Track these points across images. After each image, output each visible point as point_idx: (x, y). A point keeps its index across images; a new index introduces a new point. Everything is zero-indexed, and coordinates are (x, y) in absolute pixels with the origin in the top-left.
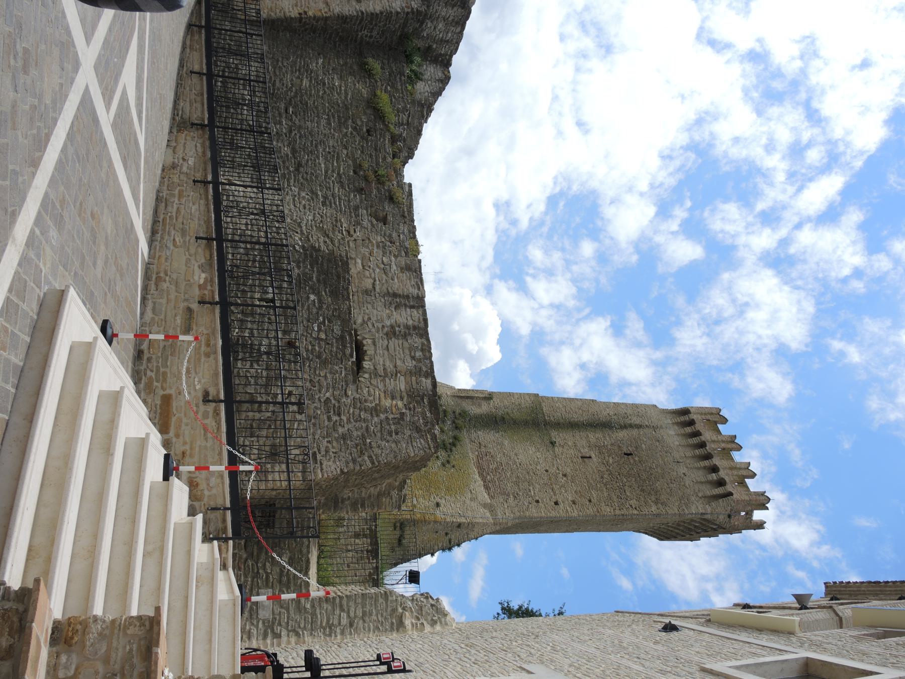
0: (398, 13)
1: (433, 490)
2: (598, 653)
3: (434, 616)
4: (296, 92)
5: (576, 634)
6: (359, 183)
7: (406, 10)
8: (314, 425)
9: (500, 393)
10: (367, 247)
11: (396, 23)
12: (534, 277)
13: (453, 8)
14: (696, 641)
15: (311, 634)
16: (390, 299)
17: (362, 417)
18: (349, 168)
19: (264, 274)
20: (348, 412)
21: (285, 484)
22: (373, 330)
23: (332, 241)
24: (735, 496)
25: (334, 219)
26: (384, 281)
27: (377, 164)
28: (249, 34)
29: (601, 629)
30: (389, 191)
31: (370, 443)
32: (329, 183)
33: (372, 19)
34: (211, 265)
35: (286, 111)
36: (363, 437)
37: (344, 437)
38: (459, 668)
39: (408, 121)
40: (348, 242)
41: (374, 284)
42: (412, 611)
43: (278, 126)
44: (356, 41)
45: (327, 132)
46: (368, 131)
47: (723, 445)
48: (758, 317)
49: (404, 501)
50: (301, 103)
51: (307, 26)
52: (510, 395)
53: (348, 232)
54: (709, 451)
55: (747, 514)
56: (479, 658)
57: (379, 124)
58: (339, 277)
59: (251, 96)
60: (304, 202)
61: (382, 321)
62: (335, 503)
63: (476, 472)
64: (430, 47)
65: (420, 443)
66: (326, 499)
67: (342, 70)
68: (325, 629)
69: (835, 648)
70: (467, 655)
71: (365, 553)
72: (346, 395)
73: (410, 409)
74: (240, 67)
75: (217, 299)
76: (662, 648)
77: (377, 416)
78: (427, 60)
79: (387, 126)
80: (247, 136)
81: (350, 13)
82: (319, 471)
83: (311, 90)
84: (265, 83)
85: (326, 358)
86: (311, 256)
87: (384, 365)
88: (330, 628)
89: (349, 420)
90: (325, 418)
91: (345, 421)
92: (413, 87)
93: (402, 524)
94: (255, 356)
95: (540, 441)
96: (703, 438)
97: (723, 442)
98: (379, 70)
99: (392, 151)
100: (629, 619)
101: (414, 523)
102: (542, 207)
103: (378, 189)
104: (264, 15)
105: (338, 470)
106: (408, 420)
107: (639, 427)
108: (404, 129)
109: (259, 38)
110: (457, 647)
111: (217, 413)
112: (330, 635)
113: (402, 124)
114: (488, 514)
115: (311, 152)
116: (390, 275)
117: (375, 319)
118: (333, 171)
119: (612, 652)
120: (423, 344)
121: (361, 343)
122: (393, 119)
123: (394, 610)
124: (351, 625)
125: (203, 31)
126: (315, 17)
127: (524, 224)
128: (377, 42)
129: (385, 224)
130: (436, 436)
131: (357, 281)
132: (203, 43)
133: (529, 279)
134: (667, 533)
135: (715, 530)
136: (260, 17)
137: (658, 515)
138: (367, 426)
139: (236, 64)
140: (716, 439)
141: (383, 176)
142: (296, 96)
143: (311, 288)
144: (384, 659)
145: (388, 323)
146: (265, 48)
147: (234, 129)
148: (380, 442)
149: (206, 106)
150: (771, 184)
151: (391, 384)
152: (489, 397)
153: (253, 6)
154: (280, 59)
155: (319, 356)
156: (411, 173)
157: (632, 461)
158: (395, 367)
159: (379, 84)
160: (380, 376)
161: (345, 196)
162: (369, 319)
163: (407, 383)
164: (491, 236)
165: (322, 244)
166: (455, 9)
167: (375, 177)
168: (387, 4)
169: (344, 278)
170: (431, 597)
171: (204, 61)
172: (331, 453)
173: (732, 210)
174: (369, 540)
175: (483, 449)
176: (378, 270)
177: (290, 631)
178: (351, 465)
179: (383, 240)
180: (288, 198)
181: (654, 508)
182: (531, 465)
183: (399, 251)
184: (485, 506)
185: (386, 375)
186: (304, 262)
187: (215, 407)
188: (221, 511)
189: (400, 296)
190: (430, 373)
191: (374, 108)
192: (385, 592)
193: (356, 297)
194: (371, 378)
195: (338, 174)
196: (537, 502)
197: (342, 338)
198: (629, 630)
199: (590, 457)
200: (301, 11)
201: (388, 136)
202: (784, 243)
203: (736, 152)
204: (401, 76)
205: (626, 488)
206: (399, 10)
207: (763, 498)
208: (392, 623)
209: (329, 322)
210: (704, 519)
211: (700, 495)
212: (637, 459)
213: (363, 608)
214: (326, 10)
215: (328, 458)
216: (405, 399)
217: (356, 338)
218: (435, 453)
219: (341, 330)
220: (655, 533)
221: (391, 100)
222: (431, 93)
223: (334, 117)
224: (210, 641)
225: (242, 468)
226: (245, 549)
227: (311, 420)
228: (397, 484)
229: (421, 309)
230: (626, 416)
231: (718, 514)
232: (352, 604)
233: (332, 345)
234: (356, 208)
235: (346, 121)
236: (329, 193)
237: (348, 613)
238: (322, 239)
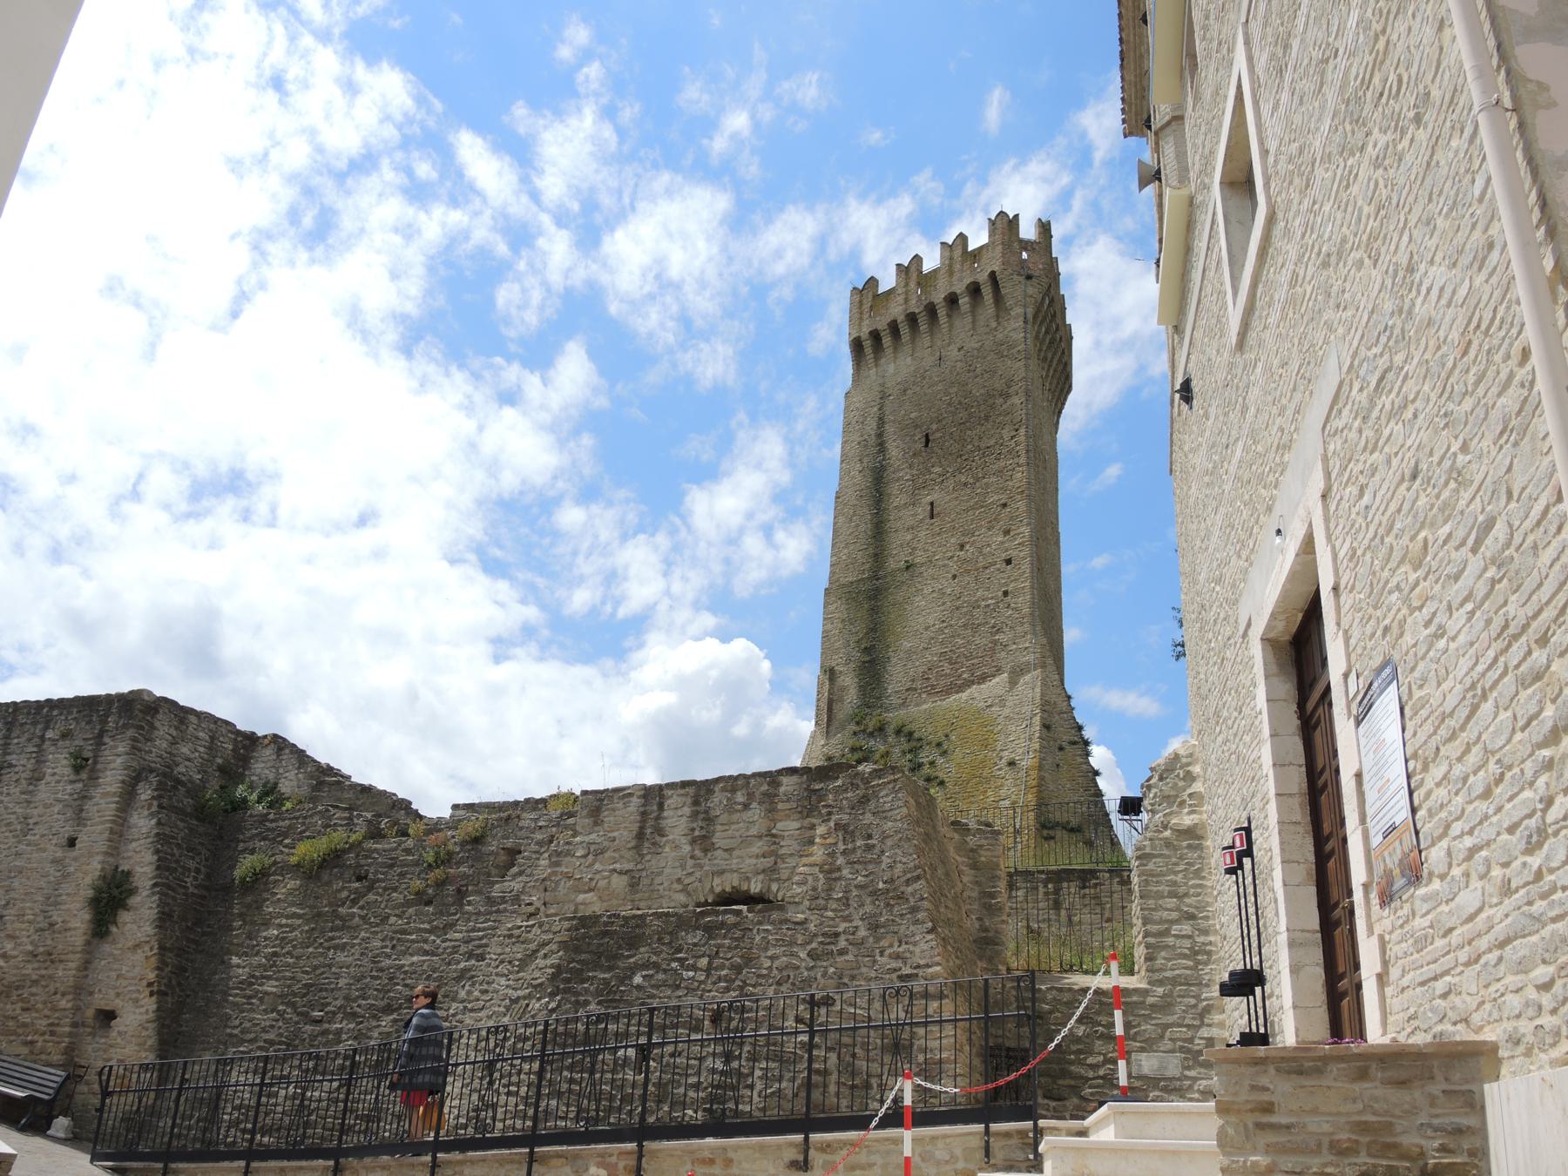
0: (159, 823)
1: (987, 771)
2: (1222, 510)
3: (1178, 776)
4: (287, 1004)
5: (1198, 543)
6: (448, 895)
7: (154, 809)
8: (853, 978)
9: (822, 654)
10: (557, 883)
11: (176, 827)
12: (617, 603)
13: (155, 728)
14: (1203, 353)
15: (1207, 985)
16: (646, 844)
17: (840, 895)
18: (422, 914)
19: (593, 1064)
20: (833, 919)
21: (949, 1030)
22: (698, 875)
23: (544, 944)
24: (996, 269)
25: (507, 941)
26: (616, 855)
27: (416, 863)
28: (182, 1083)
29: (1191, 501)
30: (463, 843)
31: (885, 883)
32: (445, 949)
33: (168, 869)
34: (576, 1156)
35: (318, 1022)
36: (874, 893)
37: (874, 927)
38: (1247, 738)
39: (346, 809)
40: (547, 916)
41: (620, 873)
42: (1171, 813)
43: (344, 1037)
44: (203, 897)
45: (357, 950)
46: (359, 879)
47: (912, 285)
48: (678, 260)
49: (988, 825)
50: (305, 995)
51: (174, 982)
52: (826, 636)
53: (531, 915)
54: (922, 308)
55: (1026, 250)
56: (1234, 704)
57: (348, 859)
58: (605, 934)
59: (289, 1083)
60: (476, 993)
61: (683, 858)
62: (987, 944)
63: (957, 696)
64: (221, 769)
65: (886, 799)
66: (980, 958)
67: (253, 923)
68: (1198, 963)
69: (1209, 137)
70: (1230, 722)
71: (1087, 891)
72: (805, 921)
73: (830, 813)
74: (237, 1102)
75: (632, 1146)
76: (1214, 407)
77: (839, 869)
78: (243, 775)
79: (352, 846)
80: (357, 1091)
81: (154, 906)
82: (930, 970)
83: (284, 978)
84: (266, 1059)
85: (742, 957)
86: (568, 981)
87: (757, 857)
88: (1197, 953)
89: (847, 919)
90: (840, 959)
91: (847, 925)
92: (288, 799)
93: (1044, 826)
94: (732, 1083)
95: (905, 588)
96: (901, 318)
97: (907, 285)
98: (254, 857)
99: (396, 836)
100: (1178, 456)
101: (1041, 805)
102: (503, 586)
103: (459, 864)
104: (150, 1058)
105: (929, 937)
106: (847, 817)
107: (881, 421)
108: (359, 816)
109: (189, 1067)
110: (1220, 739)
111: (826, 1148)
112: (1209, 953)
113: (350, 819)
114: (1027, 678)
115: (391, 979)
116: (606, 844)
117: (679, 870)
118: (426, 941)
119: (1220, 487)
120: (723, 790)
121: (719, 895)
122: (339, 837)
123: (1168, 843)
124: (1192, 917)
125: (173, 1166)
126: (158, 968)
127: (531, 613)
128: (206, 860)
129: (520, 852)
130: (875, 770)
131: (615, 902)
132: (193, 1165)
133: (622, 612)
134: (1059, 379)
135: (1052, 301)
136: (154, 1065)
137: (1027, 393)
138: (856, 887)
139: (233, 1109)
140: (903, 297)
141: (437, 853)
142: (293, 1005)
143: (622, 981)
144: (1232, 862)
145: (687, 848)
146: (207, 1057)
147: (344, 1114)
148: (883, 866)
149: (304, 1163)
150: (465, 235)
151: (788, 846)
152: (830, 673)
153: (135, 1076)
154: (228, 1031)
155: (738, 969)
156: (435, 803)
157: (938, 435)
158: (760, 837)
159: (279, 858)
160: (776, 863)
161: (469, 920)
162: (679, 880)
163: (788, 817)
164: (551, 670)
165: (549, 962)
166: (157, 724)
167: (438, 867)
168: (142, 842)
169: (606, 924)
170: (1148, 780)
171: (226, 1164)
172: (901, 949)
173: (505, 295)
174: (1065, 885)
175: (918, 684)
176: (597, 866)
177: (1202, 1022)
178: (921, 915)
179: (546, 855)
180: (468, 1021)
181: (1016, 400)
182: (944, 604)
183: (567, 827)
184: (1013, 683)
185: (774, 853)
186: (577, 994)
187: (816, 1149)
188: (992, 1140)
189: (642, 828)
190: (772, 778)
191: (321, 867)
192: (1138, 858)
193: (642, 904)
194: (778, 880)
195: (430, 932)
196: (1006, 593)
197: (709, 930)
198: (1191, 456)
199: (932, 504)
200: (147, 993)
201: (370, 845)
202: (561, 220)
203: (414, 286)
204: (268, 820)
205: (983, 445)
206: (154, 822)
207: (998, 222)
208: (1189, 847)
209: (680, 952)
210: (1035, 317)
211: (994, 324)
212: (934, 427)
213: (1163, 897)
214: (147, 948)
215: (908, 955)
216: (814, 821)
217: (710, 904)
218: (903, 772)
219: (694, 931)
220: (1059, 398)
221: (308, 837)
222: (299, 768)
223: (332, 939)
224: (1176, 1153)
225: (908, 1101)
226: (1065, 1099)
227: (845, 984)
228: (956, 836)
229: (665, 792)
230: (863, 444)
231: (1026, 296)
232: (1157, 915)
233: (719, 946)
234: (490, 901)
235: (342, 918)
236: (463, 949)
237: (1172, 922)
238: (540, 962)
